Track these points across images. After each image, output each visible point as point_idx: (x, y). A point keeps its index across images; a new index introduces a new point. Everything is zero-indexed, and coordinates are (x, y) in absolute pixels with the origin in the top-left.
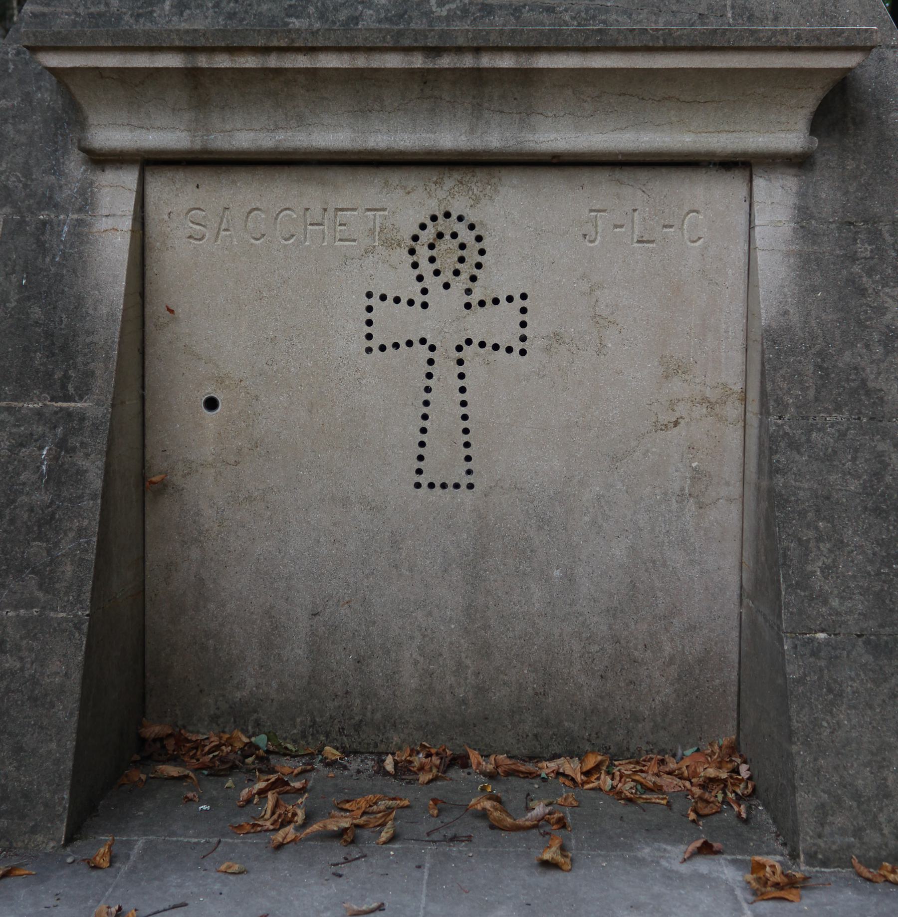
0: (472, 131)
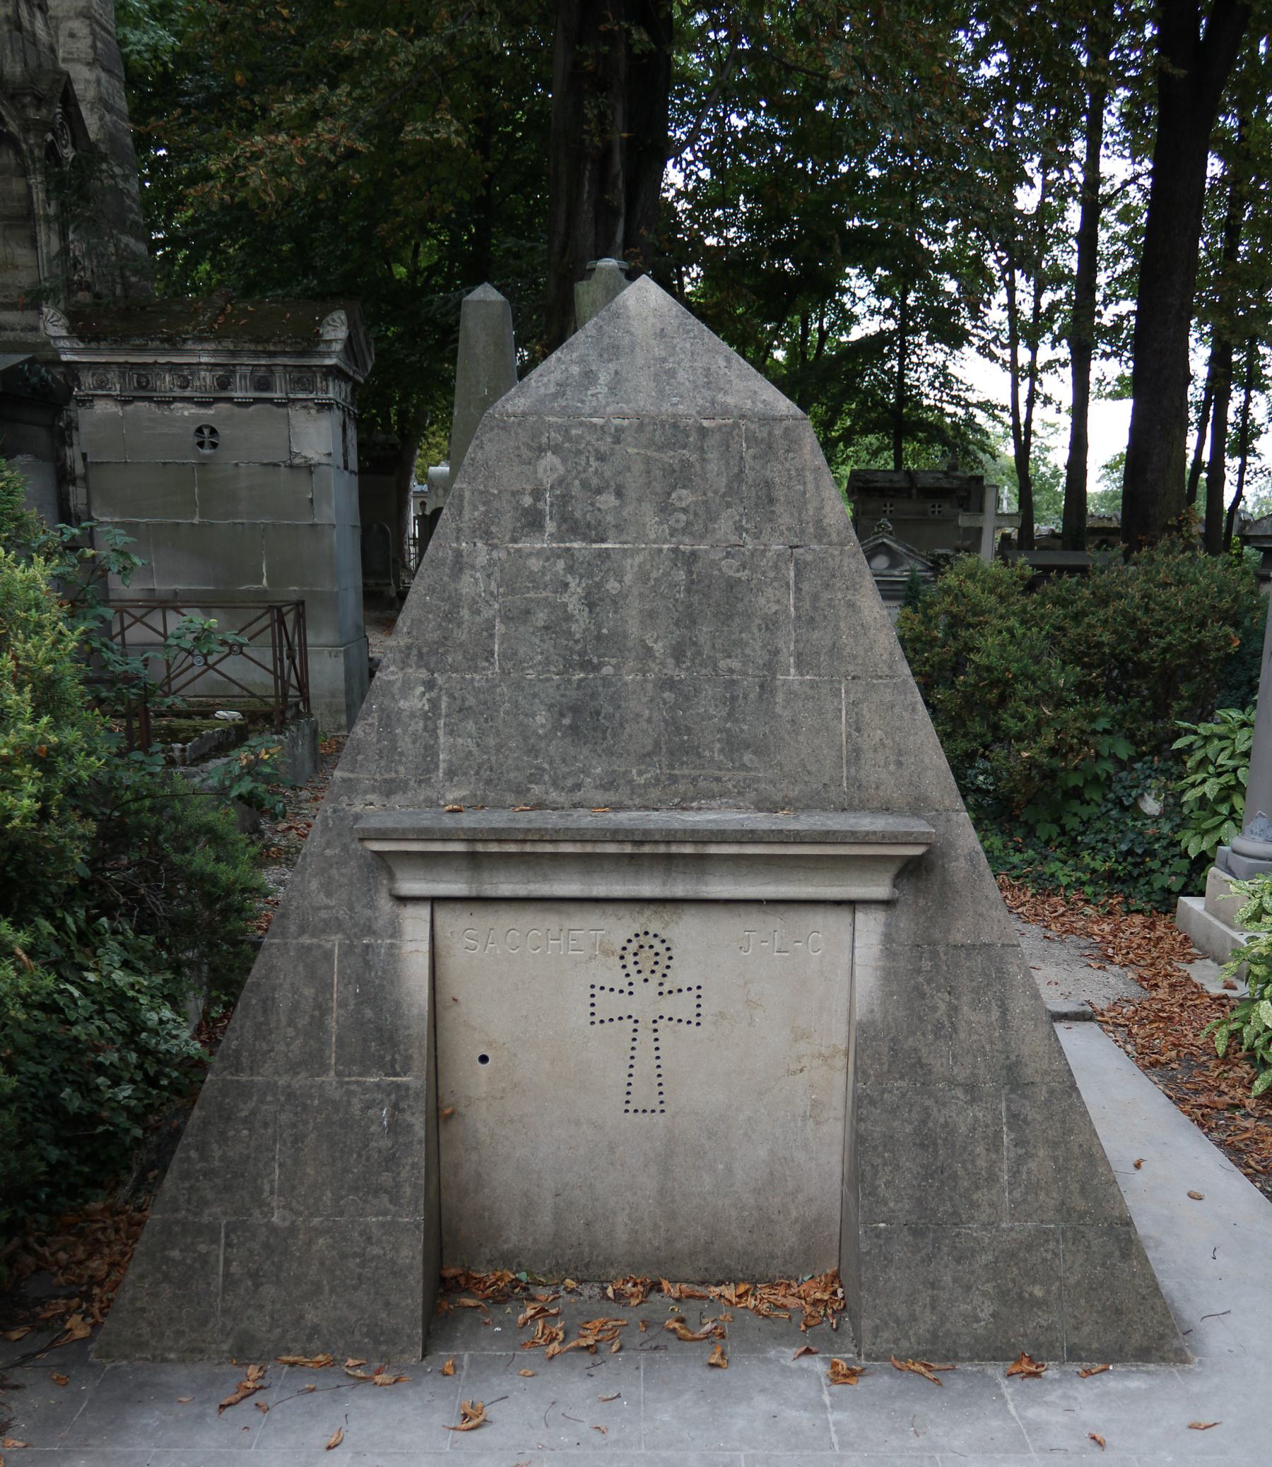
0: (664, 884)
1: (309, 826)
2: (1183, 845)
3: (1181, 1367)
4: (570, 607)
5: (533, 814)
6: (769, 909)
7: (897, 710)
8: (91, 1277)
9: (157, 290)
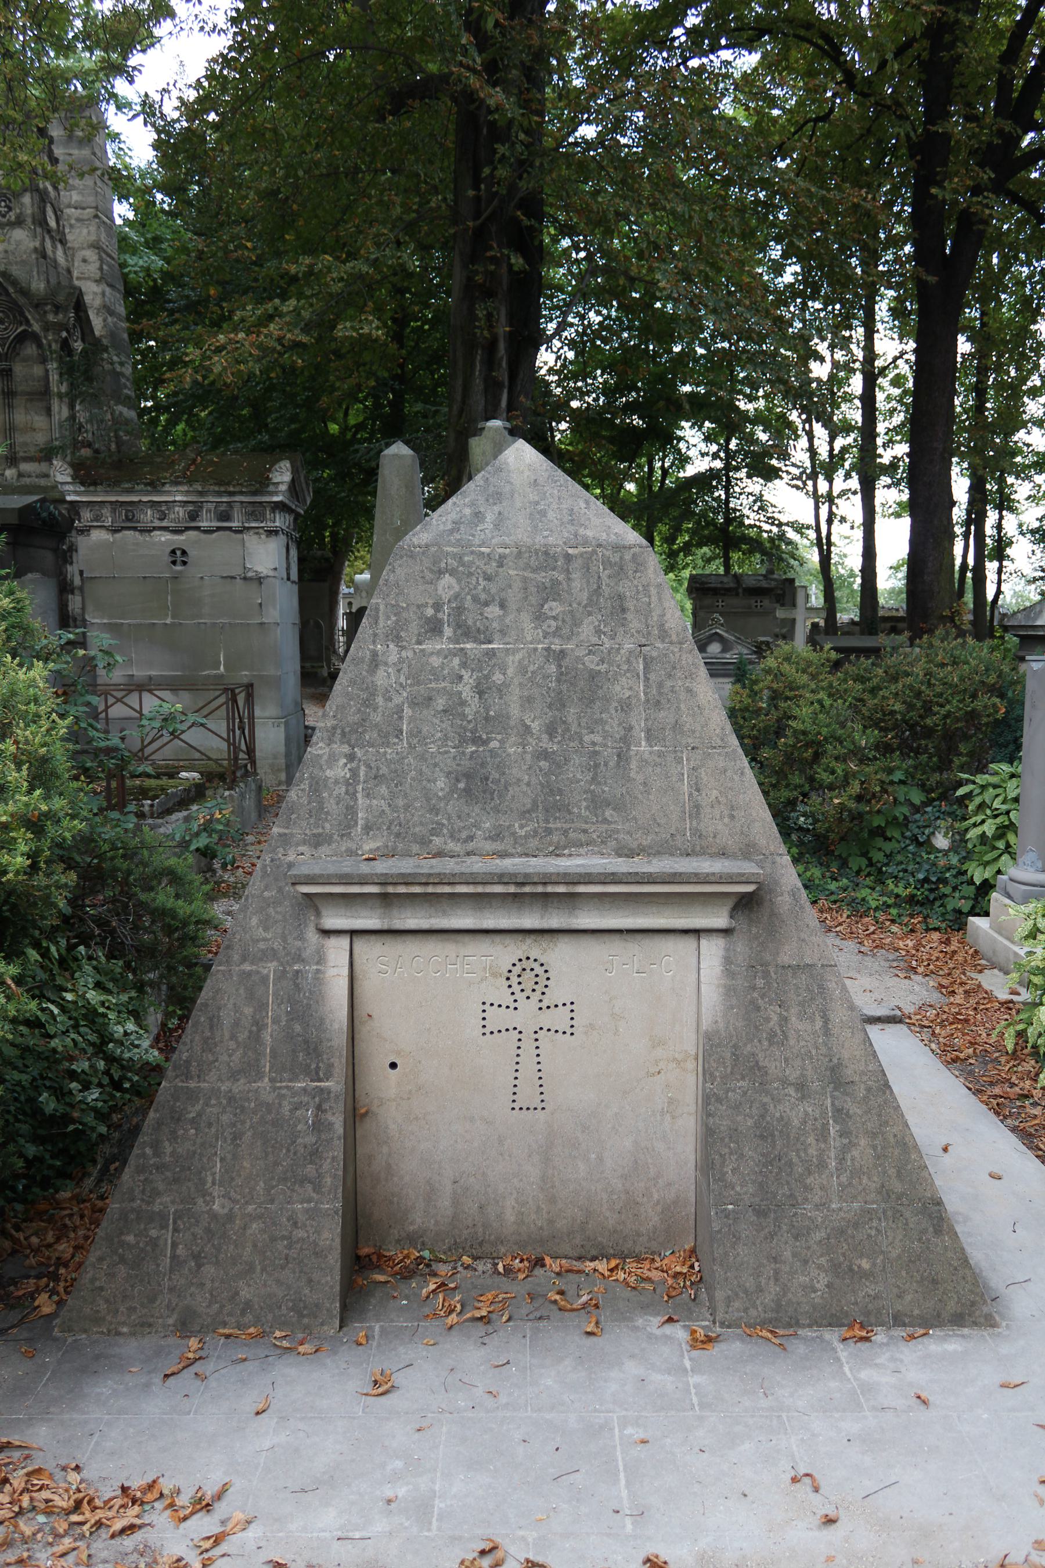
1: (254, 865)
2: (969, 873)
3: (990, 1330)
4: (464, 695)
5: (434, 861)
6: (628, 937)
7: (729, 774)
8: (58, 1259)
9: (143, 445)
